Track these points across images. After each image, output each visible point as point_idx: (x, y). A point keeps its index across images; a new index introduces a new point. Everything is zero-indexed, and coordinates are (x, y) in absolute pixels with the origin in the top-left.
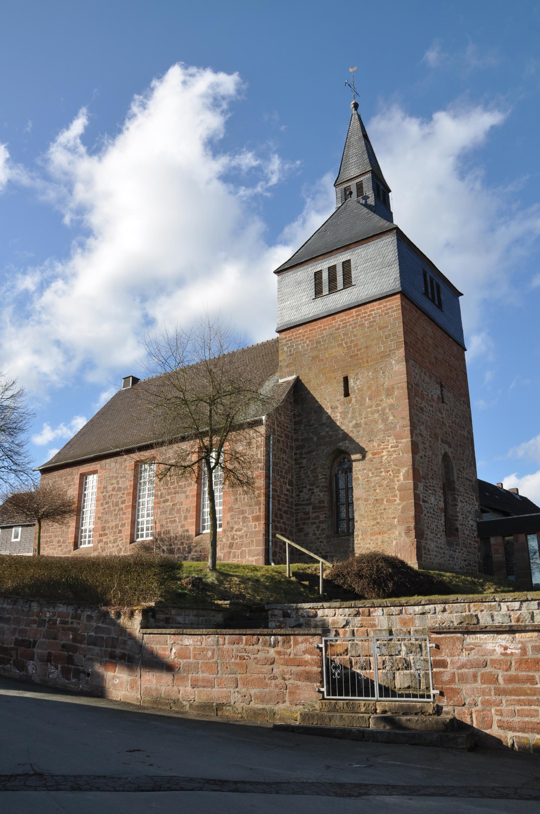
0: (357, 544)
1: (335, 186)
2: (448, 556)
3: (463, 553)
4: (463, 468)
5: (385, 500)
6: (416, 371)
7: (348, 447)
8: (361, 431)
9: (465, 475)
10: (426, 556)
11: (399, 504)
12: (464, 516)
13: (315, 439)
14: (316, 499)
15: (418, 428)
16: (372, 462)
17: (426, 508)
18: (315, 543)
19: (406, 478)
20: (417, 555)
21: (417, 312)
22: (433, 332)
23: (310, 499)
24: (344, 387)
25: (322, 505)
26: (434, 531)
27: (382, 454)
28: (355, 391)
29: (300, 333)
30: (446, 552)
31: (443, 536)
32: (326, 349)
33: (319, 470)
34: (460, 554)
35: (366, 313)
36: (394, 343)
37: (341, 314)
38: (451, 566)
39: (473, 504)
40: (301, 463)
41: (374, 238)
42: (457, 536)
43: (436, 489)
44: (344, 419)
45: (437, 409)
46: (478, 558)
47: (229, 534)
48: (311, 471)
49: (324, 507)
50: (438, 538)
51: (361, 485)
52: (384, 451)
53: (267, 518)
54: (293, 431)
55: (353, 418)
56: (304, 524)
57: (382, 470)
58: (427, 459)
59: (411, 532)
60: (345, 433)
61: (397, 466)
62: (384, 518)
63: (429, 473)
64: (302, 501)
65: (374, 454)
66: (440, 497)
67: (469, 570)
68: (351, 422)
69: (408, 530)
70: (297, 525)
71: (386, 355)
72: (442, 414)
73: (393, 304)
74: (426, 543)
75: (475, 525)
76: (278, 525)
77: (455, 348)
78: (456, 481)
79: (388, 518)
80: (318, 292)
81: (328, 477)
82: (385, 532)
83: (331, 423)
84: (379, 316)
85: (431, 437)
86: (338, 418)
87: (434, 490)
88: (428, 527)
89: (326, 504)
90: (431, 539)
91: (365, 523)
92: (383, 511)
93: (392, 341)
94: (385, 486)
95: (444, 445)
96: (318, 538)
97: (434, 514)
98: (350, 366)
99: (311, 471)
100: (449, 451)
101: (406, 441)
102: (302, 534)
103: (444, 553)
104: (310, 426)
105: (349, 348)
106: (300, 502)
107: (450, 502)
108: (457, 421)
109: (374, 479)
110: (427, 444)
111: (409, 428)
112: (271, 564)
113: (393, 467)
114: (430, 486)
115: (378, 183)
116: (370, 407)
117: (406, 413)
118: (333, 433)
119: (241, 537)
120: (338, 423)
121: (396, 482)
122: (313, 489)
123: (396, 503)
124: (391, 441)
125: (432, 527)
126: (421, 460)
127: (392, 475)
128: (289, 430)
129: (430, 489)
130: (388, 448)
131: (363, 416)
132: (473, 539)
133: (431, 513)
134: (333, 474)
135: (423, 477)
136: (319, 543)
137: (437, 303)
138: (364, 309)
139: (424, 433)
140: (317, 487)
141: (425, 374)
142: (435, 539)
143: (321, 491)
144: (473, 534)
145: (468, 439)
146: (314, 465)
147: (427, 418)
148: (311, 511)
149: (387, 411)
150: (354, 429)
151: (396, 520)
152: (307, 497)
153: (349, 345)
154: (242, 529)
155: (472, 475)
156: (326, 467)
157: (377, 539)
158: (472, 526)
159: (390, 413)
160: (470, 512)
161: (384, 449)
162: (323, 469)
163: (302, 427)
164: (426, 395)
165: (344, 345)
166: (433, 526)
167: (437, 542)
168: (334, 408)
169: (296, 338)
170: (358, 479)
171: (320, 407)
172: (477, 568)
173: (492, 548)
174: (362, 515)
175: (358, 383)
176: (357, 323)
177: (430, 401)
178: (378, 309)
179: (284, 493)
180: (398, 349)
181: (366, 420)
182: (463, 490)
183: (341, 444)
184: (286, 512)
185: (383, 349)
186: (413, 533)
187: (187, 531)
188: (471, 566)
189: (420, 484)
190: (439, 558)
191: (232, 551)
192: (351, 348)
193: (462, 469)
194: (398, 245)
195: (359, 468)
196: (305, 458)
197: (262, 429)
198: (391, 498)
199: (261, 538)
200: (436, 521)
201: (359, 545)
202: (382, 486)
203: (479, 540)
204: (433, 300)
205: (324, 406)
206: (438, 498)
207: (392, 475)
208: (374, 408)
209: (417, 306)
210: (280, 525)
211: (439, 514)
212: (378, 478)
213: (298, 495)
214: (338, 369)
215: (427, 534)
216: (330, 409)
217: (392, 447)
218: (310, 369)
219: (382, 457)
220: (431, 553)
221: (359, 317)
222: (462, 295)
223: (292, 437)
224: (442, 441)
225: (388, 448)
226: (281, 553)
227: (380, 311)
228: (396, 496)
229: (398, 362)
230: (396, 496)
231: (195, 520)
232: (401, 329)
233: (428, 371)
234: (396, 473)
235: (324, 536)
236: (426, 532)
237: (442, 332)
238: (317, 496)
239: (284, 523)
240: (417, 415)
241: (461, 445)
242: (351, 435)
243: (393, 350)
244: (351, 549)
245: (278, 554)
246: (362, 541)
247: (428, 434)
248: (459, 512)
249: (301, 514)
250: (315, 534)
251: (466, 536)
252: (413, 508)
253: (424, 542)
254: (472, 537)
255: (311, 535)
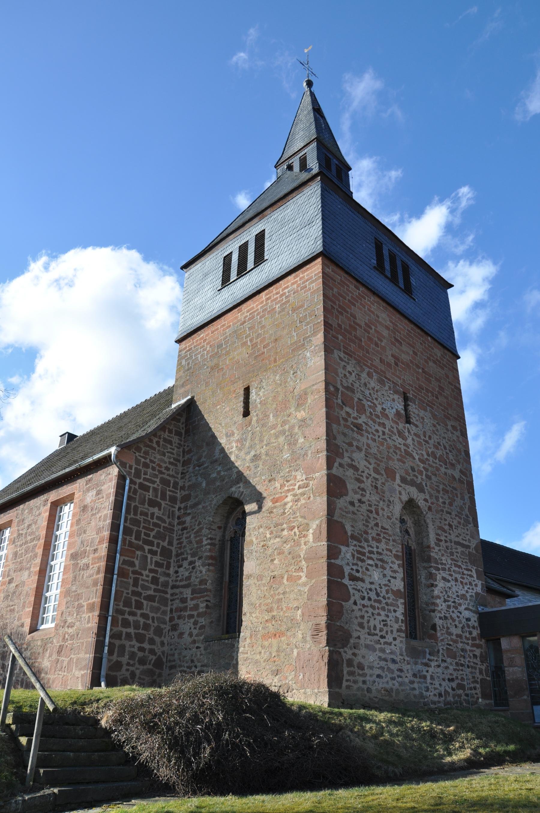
0: (243, 653)
1: (276, 167)
2: (409, 675)
3: (447, 668)
4: (450, 526)
5: (286, 577)
6: (349, 368)
7: (243, 492)
8: (261, 466)
9: (453, 537)
10: (351, 678)
11: (305, 584)
12: (450, 603)
13: (204, 484)
14: (196, 578)
15: (346, 454)
16: (272, 515)
17: (359, 591)
18: (190, 649)
19: (316, 539)
20: (329, 676)
21: (356, 287)
22: (391, 322)
23: (189, 578)
24: (244, 402)
25: (203, 587)
26: (377, 632)
27: (286, 500)
28: (256, 406)
29: (201, 339)
30: (405, 667)
31: (399, 640)
32: (228, 353)
33: (205, 531)
34: (440, 670)
35: (277, 294)
36: (311, 327)
37: (250, 302)
38: (417, 692)
39: (471, 584)
40: (184, 522)
41: (294, 194)
42: (434, 637)
43: (385, 558)
44: (240, 450)
45: (395, 430)
46: (481, 672)
47: (61, 631)
48: (195, 533)
49: (206, 590)
50: (385, 643)
51: (254, 553)
52: (289, 494)
53: (104, 606)
54: (179, 476)
55: (251, 447)
56: (179, 617)
57: (285, 526)
58: (365, 507)
59: (320, 634)
60: (240, 471)
61: (305, 518)
62: (282, 609)
63: (370, 531)
64: (181, 581)
65: (275, 501)
66: (395, 572)
67: (460, 696)
68: (248, 453)
69: (317, 631)
70: (171, 619)
71: (300, 346)
72: (405, 439)
73: (311, 273)
74: (354, 654)
75: (474, 618)
76: (131, 618)
77: (438, 352)
78: (432, 544)
79: (288, 608)
80: (226, 280)
81: (217, 542)
82: (282, 634)
83: (224, 459)
84: (294, 293)
85: (376, 471)
86: (234, 449)
87: (381, 560)
88: (361, 625)
89: (209, 586)
90: (367, 646)
91: (257, 617)
92: (282, 596)
93: (308, 324)
94: (286, 553)
95: (407, 487)
96: (194, 642)
97: (379, 602)
98: (253, 371)
99: (195, 533)
100: (420, 498)
101: (320, 475)
102: (176, 633)
103: (401, 670)
104: (199, 466)
105: (254, 346)
106: (178, 583)
107: (423, 580)
108: (439, 453)
109: (272, 541)
110: (368, 484)
111: (325, 453)
112: (100, 686)
113: (300, 519)
114: (371, 552)
115: (328, 155)
116: (274, 427)
117: (322, 430)
118: (226, 473)
119: (72, 637)
120: (233, 458)
121: (303, 546)
122: (194, 562)
123: (300, 581)
124: (298, 477)
125: (372, 624)
126: (351, 508)
127: (298, 533)
128: (171, 472)
129: (371, 558)
130: (294, 489)
131: (265, 442)
132: (470, 642)
133: (370, 599)
134: (227, 537)
135: (353, 537)
136: (194, 650)
137: (402, 285)
138: (277, 289)
139: (362, 464)
140: (200, 558)
141: (370, 375)
142: (378, 646)
143: (204, 565)
144: (470, 633)
145: (461, 481)
146: (200, 524)
147: (370, 442)
148: (189, 596)
149: (296, 430)
150: (251, 465)
151: (299, 612)
152: (187, 574)
153: (255, 341)
154: (74, 624)
155: (468, 537)
156: (214, 527)
157: (270, 646)
158: (468, 620)
159: (300, 433)
160: (463, 597)
161: (289, 491)
162: (209, 529)
163: (191, 469)
164: (370, 407)
165: (249, 343)
166: (376, 622)
167: (383, 651)
168: (230, 436)
169: (196, 346)
170: (252, 542)
171: (214, 437)
172: (478, 691)
173: (505, 656)
174: (252, 604)
175: (261, 394)
176: (266, 309)
177: (378, 417)
178: (293, 284)
179: (149, 567)
180: (315, 334)
181: (268, 448)
182: (450, 562)
183: (233, 489)
184: (150, 598)
185: (295, 338)
186: (323, 637)
187: (22, 625)
188: (464, 690)
189: (343, 549)
190: (388, 679)
191: (61, 659)
192: (257, 346)
193: (447, 527)
194: (322, 194)
195: (254, 525)
196: (189, 514)
197: (114, 471)
198: (294, 574)
199: (91, 639)
200: (383, 613)
201: (246, 655)
202: (283, 553)
203: (483, 642)
204: (394, 279)
205: (217, 434)
206: (388, 572)
207: (298, 533)
208: (279, 428)
209: (357, 281)
210: (135, 618)
211: (389, 601)
212: (278, 540)
213: (177, 572)
214: (239, 378)
215: (359, 638)
216: (224, 437)
217: (299, 488)
218: (207, 384)
219: (286, 504)
220: (366, 671)
221: (269, 301)
222: (451, 286)
223: (176, 484)
224: (404, 480)
225: (294, 489)
226: (133, 665)
227: (295, 286)
228: (300, 569)
229: (314, 353)
230: (300, 569)
231: (31, 609)
232: (321, 306)
233: (375, 371)
234: (304, 530)
235: (202, 638)
236: (355, 634)
237: (412, 326)
238: (198, 572)
239: (144, 616)
240: (345, 435)
241: (445, 491)
242: (246, 473)
243: (309, 337)
244: (235, 662)
245: (125, 667)
246: (251, 649)
247: (371, 467)
248: (438, 597)
249: (177, 601)
250: (191, 635)
251: (454, 637)
252: (325, 591)
253: (350, 652)
254: (468, 639)
255: (186, 636)
